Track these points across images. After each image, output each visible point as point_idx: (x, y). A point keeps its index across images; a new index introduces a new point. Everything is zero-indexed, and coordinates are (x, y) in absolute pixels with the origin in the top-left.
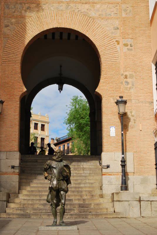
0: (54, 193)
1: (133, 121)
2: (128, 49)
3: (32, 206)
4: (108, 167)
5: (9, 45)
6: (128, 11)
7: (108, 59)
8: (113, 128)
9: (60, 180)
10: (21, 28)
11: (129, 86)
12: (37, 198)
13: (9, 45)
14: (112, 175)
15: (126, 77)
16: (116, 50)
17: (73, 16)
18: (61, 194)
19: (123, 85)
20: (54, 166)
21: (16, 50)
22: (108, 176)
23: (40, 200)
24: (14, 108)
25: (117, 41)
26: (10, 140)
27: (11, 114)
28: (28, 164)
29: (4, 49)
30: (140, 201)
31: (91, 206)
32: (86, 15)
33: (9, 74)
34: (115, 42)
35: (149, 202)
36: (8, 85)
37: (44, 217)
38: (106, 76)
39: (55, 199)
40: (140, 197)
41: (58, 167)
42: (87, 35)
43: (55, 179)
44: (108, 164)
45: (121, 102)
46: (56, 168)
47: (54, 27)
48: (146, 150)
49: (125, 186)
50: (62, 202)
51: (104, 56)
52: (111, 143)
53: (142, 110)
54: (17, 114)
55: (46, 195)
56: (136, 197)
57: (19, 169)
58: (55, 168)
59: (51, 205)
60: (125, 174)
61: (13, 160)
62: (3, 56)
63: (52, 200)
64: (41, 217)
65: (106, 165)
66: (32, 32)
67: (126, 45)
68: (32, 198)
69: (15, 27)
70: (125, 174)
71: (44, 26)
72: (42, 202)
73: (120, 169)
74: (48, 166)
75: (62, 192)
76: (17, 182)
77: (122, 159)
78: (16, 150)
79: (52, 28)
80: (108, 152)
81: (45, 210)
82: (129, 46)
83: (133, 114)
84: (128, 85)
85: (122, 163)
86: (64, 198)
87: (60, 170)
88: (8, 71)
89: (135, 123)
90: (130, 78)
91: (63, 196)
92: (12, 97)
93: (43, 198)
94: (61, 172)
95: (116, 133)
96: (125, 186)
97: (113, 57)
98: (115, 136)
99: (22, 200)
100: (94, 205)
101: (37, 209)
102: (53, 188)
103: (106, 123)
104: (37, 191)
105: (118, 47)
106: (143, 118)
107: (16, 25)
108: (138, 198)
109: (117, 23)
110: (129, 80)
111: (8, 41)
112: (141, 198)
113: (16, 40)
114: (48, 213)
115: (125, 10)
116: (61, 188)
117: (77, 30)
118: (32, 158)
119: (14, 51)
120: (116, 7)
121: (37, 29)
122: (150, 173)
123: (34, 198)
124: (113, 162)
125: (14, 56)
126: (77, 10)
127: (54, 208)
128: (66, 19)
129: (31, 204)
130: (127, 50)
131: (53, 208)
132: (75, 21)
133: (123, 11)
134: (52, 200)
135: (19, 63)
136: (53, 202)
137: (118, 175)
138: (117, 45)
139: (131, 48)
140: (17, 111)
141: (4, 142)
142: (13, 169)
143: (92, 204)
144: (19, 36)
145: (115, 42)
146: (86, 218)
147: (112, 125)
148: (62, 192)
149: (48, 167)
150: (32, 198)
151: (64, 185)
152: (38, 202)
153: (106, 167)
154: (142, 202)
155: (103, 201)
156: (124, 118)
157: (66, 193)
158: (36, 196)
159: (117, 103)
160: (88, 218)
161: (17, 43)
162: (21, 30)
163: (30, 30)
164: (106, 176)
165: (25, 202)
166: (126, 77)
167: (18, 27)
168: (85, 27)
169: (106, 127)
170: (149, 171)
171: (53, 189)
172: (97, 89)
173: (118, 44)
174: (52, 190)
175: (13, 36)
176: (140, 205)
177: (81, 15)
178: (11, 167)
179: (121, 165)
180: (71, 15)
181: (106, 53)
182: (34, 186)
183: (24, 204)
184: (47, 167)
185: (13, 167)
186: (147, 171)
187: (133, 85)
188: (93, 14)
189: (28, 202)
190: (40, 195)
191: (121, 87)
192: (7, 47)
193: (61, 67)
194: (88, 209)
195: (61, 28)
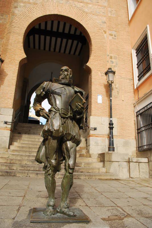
0: (54, 143)
1: (117, 93)
2: (112, 38)
3: (19, 163)
4: (95, 129)
5: (16, 21)
6: (113, 13)
7: (97, 43)
8: (101, 96)
9: (67, 118)
10: (28, 11)
11: (113, 65)
12: (26, 154)
13: (16, 21)
14: (98, 137)
15: (111, 58)
16: (103, 37)
17: (70, 9)
18: (66, 145)
19: (109, 63)
20: (57, 91)
21: (21, 25)
22: (95, 138)
23: (29, 156)
24: (13, 70)
25: (104, 31)
26: (6, 98)
27: (10, 75)
28: (24, 128)
29: (11, 23)
30: (129, 162)
31: (81, 165)
32: (81, 10)
33: (12, 43)
34: (102, 31)
35: (136, 163)
36: (10, 51)
37: (31, 176)
38: (95, 54)
39: (55, 155)
40: (129, 158)
41: (65, 93)
42: (81, 23)
43: (58, 114)
44: (95, 127)
45: (109, 72)
46: (61, 93)
47: (55, 14)
48: (128, 117)
49: (111, 147)
50: (69, 165)
51: (94, 40)
53: (124, 85)
54: (15, 75)
55: (36, 152)
56: (126, 158)
57: (11, 125)
58: (59, 94)
59: (45, 167)
60: (111, 136)
61: (6, 116)
62: (9, 28)
63: (47, 157)
64: (28, 176)
65: (94, 127)
66: (36, 14)
67: (111, 35)
68: (21, 153)
69: (23, 9)
70: (111, 136)
71: (47, 12)
72: (31, 158)
73: (107, 130)
74: (43, 91)
75: (69, 144)
76: (8, 138)
77: (110, 122)
78: (10, 107)
79: (53, 14)
80: (95, 116)
81: (33, 168)
82: (114, 36)
83: (117, 86)
84: (113, 64)
85: (110, 125)
86: (72, 156)
87: (69, 98)
88: (12, 40)
89: (118, 94)
90: (115, 59)
91: (72, 151)
92: (12, 61)
93: (32, 155)
94: (69, 104)
95: (102, 100)
96: (113, 147)
97: (101, 41)
98: (101, 103)
99: (11, 155)
100: (85, 164)
101: (25, 167)
102: (52, 132)
103: (94, 92)
104: (27, 147)
105: (105, 35)
106: (124, 90)
107: (24, 8)
108: (127, 158)
109: (104, 19)
110: (113, 60)
111: (16, 18)
112: (130, 159)
113: (22, 18)
114: (37, 171)
115: (111, 12)
116: (69, 134)
117: (73, 18)
118: (28, 126)
119: (19, 26)
120: (104, 9)
121: (41, 13)
122: (130, 137)
123: (23, 154)
125: (18, 29)
126: (75, 5)
127: (49, 175)
128: (65, 10)
129: (19, 160)
130: (112, 38)
131: (47, 174)
132: (72, 12)
133: (109, 12)
134: (47, 158)
135: (22, 35)
136: (49, 162)
137: (104, 137)
138: (104, 34)
139: (115, 37)
140: (16, 73)
142: (5, 124)
143: (82, 164)
144: (25, 15)
145: (102, 31)
146: (78, 178)
147: (99, 94)
148: (69, 144)
149: (44, 93)
150: (21, 153)
151: (74, 130)
152: (26, 158)
153: (93, 129)
154: (131, 164)
155: (92, 161)
156: (109, 87)
157: (77, 145)
158: (26, 152)
159: (106, 74)
160: (81, 179)
161: (22, 20)
162: (27, 11)
163: (34, 13)
164: (93, 137)
165: (14, 157)
166: (111, 58)
167: (25, 10)
168: (80, 18)
169: (94, 94)
170: (130, 136)
171: (51, 136)
172: (88, 63)
173: (105, 33)
174: (49, 137)
175: (20, 15)
176: (139, 167)
177: (77, 9)
178: (3, 122)
179: (109, 127)
180: (69, 8)
181: (96, 38)
182: (26, 143)
183: (12, 160)
184: (42, 92)
185: (6, 123)
186: (128, 136)
187: (117, 64)
188: (86, 10)
189: (17, 158)
190: (30, 151)
191: (107, 65)
192: (14, 22)
193: (52, 73)
194: (80, 169)
195: (60, 15)
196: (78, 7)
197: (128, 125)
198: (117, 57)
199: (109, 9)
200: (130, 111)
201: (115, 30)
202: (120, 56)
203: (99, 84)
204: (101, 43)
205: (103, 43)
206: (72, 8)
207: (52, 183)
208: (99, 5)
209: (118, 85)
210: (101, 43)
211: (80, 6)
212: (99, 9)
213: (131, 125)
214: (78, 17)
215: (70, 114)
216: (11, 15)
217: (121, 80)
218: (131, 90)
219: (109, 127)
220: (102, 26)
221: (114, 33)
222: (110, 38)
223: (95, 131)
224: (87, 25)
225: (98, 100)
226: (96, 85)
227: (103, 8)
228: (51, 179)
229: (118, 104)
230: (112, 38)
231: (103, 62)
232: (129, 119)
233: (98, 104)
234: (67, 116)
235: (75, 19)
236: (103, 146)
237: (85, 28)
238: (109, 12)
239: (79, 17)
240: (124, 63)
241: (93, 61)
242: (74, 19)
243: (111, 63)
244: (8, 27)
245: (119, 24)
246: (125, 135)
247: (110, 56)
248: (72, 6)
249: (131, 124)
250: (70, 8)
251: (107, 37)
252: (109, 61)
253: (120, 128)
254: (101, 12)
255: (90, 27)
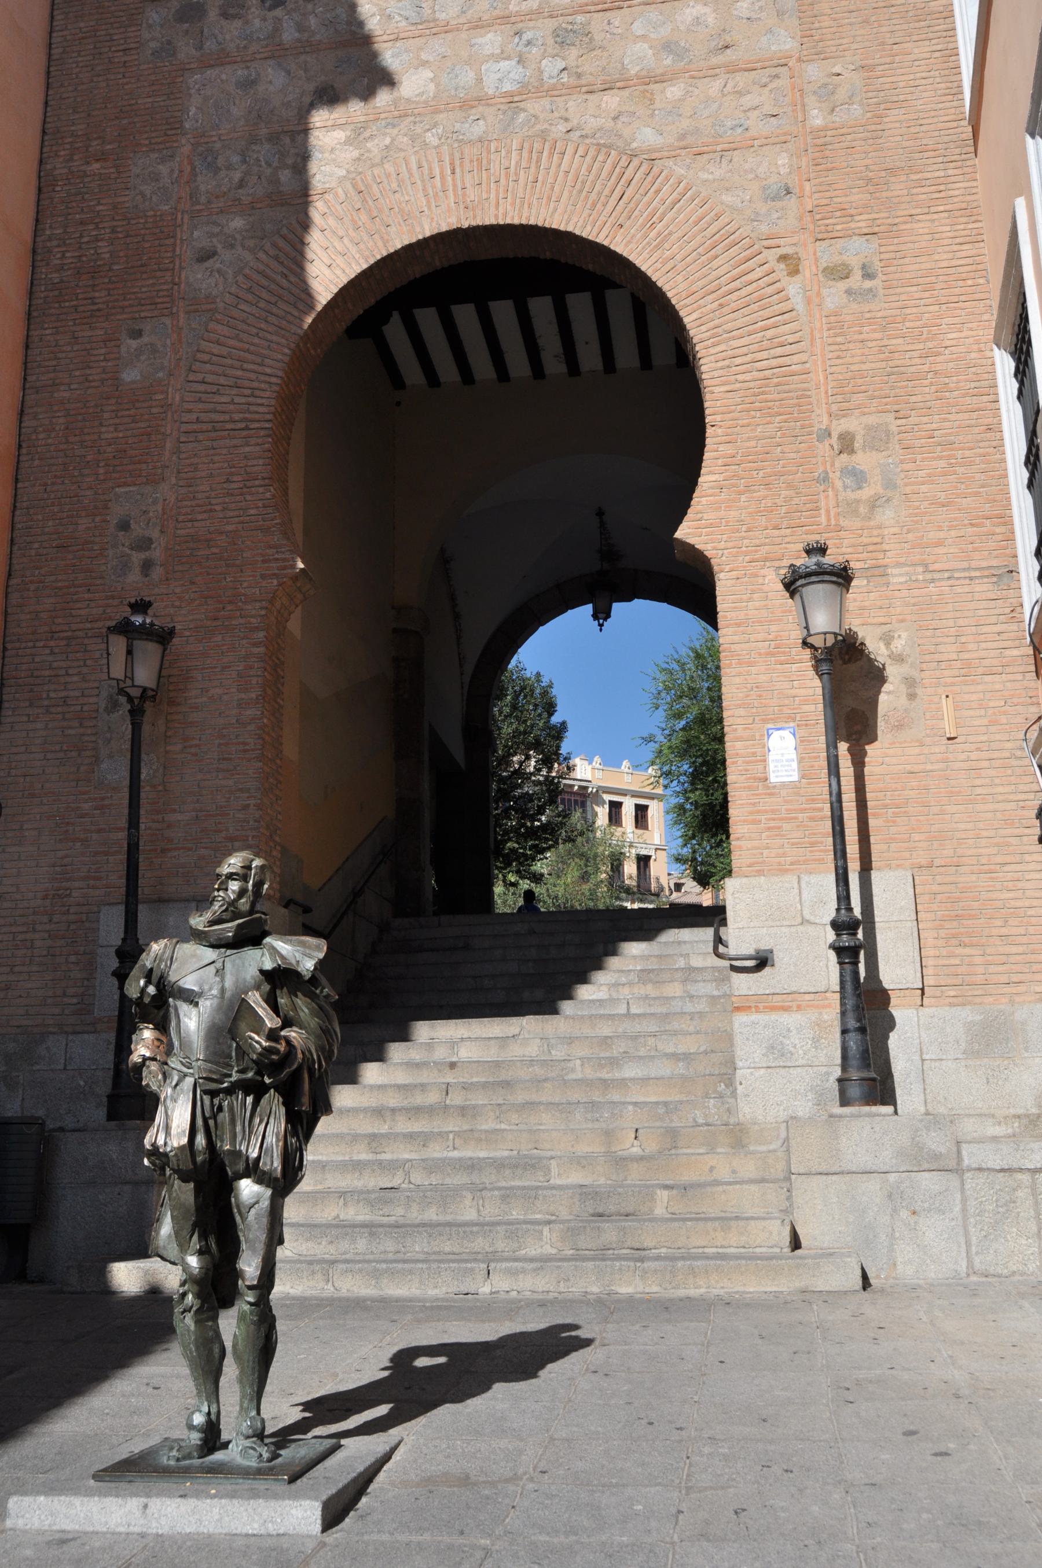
2: (849, 292)
4: (762, 962)
7: (738, 361)
8: (786, 734)
11: (866, 493)
15: (847, 444)
17: (539, 161)
21: (251, 367)
25: (783, 258)
32: (609, 147)
38: (729, 450)
44: (764, 946)
48: (995, 850)
52: (772, 824)
65: (751, 952)
67: (838, 272)
71: (392, 230)
74: (149, 982)
79: (433, 238)
80: (760, 873)
82: (857, 274)
84: (860, 488)
85: (838, 935)
90: (872, 448)
95: (801, 760)
97: (766, 344)
105: (793, 288)
106: (958, 664)
110: (863, 460)
115: (826, 92)
119: (239, 373)
122: (1022, 988)
124: (793, 929)
126: (562, 127)
128: (503, 181)
138: (785, 281)
139: (868, 284)
141: (190, 849)
145: (772, 264)
149: (151, 990)
155: (734, 1172)
166: (847, 444)
170: (1015, 978)
173: (794, 272)
187: (889, 484)
191: (822, 504)
195: (478, 227)
196: (587, 131)
197: (1000, 904)
198: (888, 433)
199: (814, 72)
200: (1013, 805)
201: (861, 224)
202: (913, 420)
203: (772, 654)
204: (764, 355)
205: (779, 351)
206: (551, 155)
207: (196, 1339)
208: (732, 69)
209: (904, 635)
210: (764, 355)
211: (601, 121)
212: (740, 94)
213: (1018, 904)
214: (594, 205)
215: (237, 1072)
216: (182, 315)
217: (932, 589)
218: (1008, 652)
219: (833, 947)
220: (764, 229)
221: (856, 251)
222: (834, 295)
223: (767, 970)
224: (658, 247)
225: (772, 766)
226: (751, 664)
227: (762, 76)
228: (192, 1328)
229: (916, 768)
230: (849, 292)
231: (791, 493)
232: (999, 859)
233: (772, 790)
234: (226, 1085)
235: (577, 232)
236: (824, 1069)
237: (649, 273)
238: (811, 101)
239: (599, 206)
240: (942, 463)
241: (723, 496)
242: (570, 229)
243: (845, 487)
244: (177, 398)
245: (891, 171)
246: (979, 979)
247: (835, 435)
248: (543, 135)
249: (1019, 894)
250: (534, 156)
251: (808, 302)
252: (835, 476)
253: (942, 933)
254: (753, 120)
255: (678, 257)
